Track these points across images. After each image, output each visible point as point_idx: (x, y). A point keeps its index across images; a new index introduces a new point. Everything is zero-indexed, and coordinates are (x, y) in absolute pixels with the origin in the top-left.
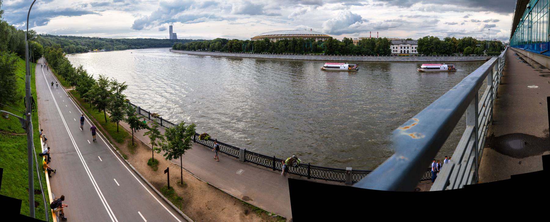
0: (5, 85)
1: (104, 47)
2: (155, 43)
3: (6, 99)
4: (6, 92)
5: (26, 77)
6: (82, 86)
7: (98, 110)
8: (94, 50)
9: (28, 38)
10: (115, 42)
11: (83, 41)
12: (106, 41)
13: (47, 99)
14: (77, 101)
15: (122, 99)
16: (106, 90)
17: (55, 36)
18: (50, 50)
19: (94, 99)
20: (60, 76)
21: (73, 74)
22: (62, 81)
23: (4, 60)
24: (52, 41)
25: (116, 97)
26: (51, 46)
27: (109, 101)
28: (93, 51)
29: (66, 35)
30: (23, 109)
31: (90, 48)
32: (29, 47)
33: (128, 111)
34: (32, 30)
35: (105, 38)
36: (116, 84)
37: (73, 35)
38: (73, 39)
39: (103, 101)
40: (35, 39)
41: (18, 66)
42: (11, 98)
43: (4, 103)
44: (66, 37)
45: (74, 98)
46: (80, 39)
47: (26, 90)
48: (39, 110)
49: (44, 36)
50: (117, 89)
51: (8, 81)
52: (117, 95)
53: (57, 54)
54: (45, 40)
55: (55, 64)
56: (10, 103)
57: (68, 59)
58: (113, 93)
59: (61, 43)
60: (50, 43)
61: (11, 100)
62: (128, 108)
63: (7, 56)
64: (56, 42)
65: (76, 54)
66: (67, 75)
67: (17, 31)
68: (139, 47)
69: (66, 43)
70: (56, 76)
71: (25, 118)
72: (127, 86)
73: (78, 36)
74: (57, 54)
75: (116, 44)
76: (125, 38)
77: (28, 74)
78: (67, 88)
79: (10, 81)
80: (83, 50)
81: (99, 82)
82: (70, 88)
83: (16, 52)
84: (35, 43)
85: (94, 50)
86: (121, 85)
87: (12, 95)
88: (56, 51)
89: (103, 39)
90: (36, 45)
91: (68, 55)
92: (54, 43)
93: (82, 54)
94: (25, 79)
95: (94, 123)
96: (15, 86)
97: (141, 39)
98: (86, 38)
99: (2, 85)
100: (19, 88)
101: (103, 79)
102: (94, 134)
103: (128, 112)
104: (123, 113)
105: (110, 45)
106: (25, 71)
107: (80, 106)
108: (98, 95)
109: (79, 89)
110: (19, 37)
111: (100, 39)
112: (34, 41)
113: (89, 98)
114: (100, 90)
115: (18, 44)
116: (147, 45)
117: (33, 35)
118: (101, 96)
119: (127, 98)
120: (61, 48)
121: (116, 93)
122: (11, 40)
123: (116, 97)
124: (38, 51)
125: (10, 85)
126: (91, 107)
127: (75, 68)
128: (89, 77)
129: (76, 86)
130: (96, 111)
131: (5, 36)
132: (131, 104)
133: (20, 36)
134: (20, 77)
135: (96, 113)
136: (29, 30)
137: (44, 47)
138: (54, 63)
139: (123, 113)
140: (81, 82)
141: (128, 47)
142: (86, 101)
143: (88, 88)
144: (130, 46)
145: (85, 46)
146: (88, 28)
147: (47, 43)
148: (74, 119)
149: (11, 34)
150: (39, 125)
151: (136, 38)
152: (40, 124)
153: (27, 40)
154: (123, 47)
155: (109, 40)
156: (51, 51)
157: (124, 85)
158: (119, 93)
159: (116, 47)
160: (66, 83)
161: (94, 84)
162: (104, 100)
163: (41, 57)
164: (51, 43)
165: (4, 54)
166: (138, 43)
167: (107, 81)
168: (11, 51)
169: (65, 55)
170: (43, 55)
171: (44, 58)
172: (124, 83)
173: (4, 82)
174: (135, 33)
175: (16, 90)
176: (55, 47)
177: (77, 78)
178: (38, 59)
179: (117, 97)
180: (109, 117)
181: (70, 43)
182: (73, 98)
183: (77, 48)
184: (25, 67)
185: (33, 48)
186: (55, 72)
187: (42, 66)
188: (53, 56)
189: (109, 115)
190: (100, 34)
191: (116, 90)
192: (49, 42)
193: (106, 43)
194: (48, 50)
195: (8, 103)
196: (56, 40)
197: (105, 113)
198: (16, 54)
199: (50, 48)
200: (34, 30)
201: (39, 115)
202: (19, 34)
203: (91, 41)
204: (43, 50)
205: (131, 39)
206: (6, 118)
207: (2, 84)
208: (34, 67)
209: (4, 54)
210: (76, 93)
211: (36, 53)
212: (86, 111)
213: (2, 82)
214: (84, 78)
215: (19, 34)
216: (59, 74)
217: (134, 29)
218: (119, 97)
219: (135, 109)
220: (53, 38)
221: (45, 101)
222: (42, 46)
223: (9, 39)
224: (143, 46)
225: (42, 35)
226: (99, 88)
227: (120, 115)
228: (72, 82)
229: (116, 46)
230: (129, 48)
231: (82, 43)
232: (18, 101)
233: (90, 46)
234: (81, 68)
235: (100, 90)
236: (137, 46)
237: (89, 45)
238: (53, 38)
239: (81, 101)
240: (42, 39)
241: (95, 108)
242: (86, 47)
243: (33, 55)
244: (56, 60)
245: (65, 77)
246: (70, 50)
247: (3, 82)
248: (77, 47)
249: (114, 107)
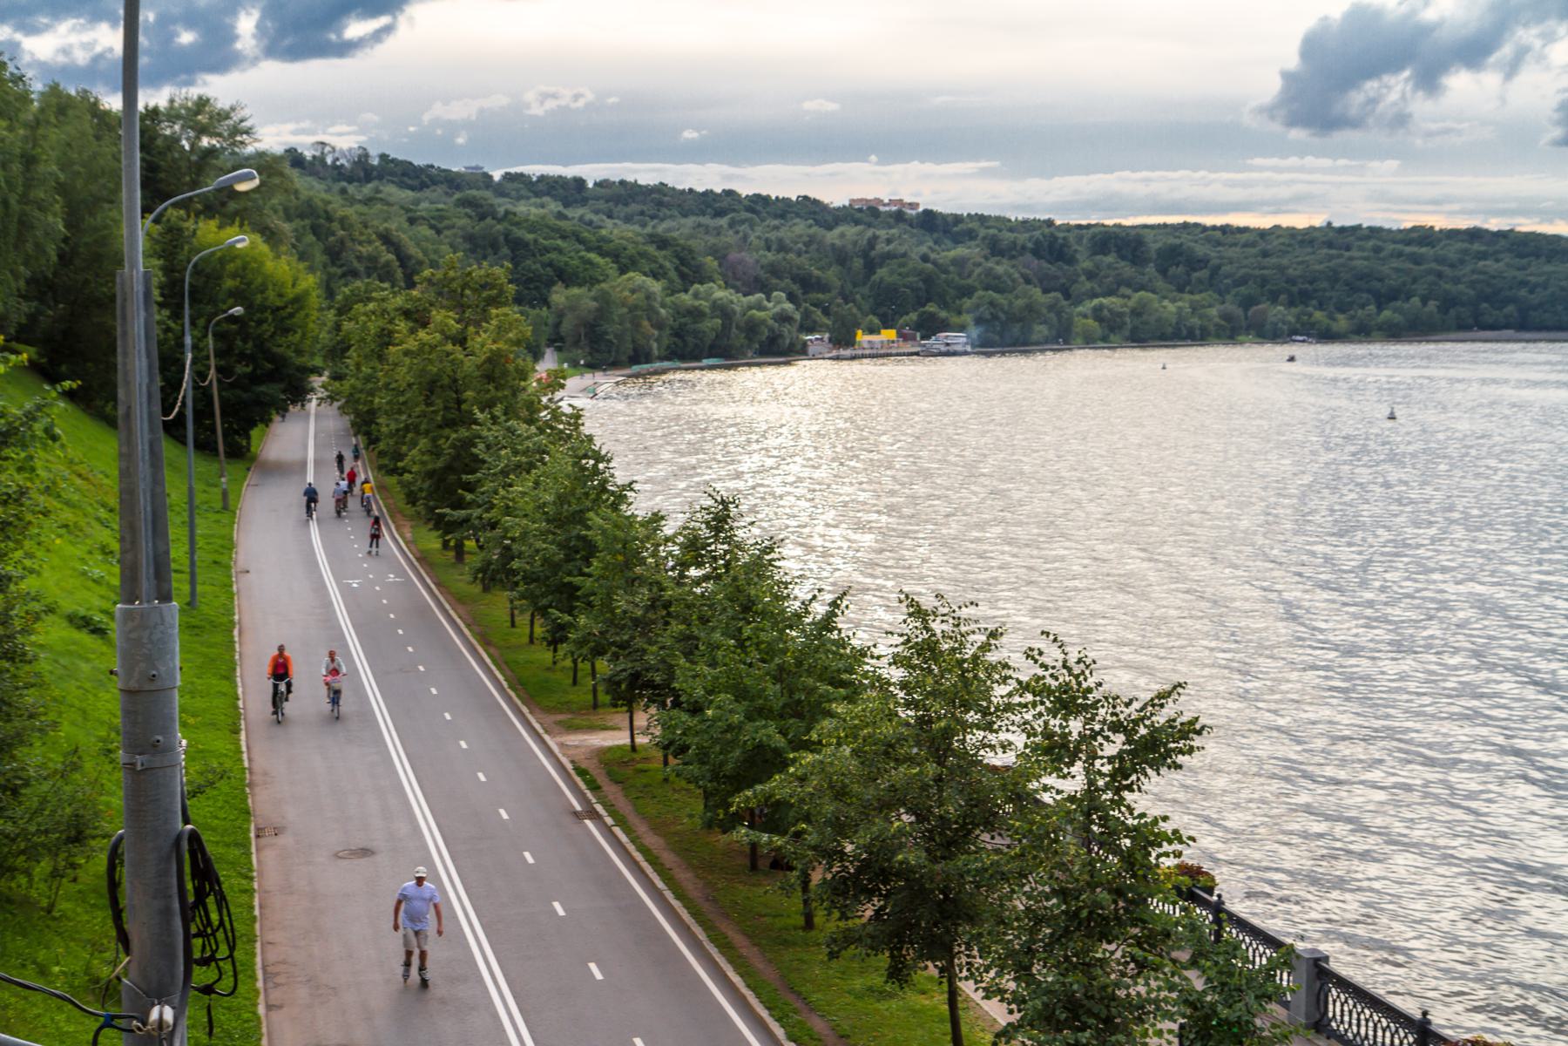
1: (967, 303)
2: (1523, 283)
6: (723, 708)
7: (884, 959)
8: (862, 337)
9: (155, 191)
10: (1086, 264)
12: (996, 249)
13: (359, 841)
14: (668, 858)
15: (1135, 862)
16: (970, 762)
17: (452, 181)
18: (402, 326)
19: (849, 848)
20: (499, 604)
21: (632, 583)
24: (424, 231)
25: (1069, 841)
26: (411, 285)
27: (1004, 877)
29: (569, 172)
31: (818, 314)
33: (1199, 985)
34: (202, 103)
35: (982, 219)
36: (1085, 708)
37: (645, 174)
39: (937, 867)
40: (232, 206)
45: (642, 829)
46: (719, 213)
47: (130, 767)
48: (272, 956)
49: (338, 173)
50: (1093, 756)
53: (469, 365)
54: (350, 211)
55: (452, 478)
57: (586, 430)
58: (1046, 798)
59: (517, 245)
62: (1194, 963)
64: (470, 238)
66: (569, 596)
67: (25, 98)
68: (1342, 322)
69: (571, 255)
70: (458, 600)
72: (1191, 729)
73: (700, 189)
74: (469, 365)
75: (1091, 275)
76: (1192, 219)
77: (146, 584)
80: (752, 328)
81: (897, 674)
84: (242, 240)
85: (862, 337)
86: (1125, 713)
88: (461, 341)
89: (958, 219)
90: (246, 267)
91: (588, 379)
92: (445, 248)
97: (1375, 232)
98: (783, 209)
101: (946, 646)
103: (1192, 1002)
105: (1037, 292)
107: (695, 914)
108: (886, 806)
109: (692, 740)
110: (49, 167)
111: (930, 221)
112: (228, 219)
113: (798, 835)
115: (39, 247)
116: (1432, 305)
117: (211, 152)
118: (921, 818)
119: (1190, 856)
120: (512, 312)
121: (1072, 799)
123: (1069, 841)
126: (809, 924)
127: (657, 518)
132: (1231, 915)
134: (68, 606)
135: (858, 983)
136: (141, 107)
137: (330, 293)
138: (440, 464)
141: (1227, 317)
142: (764, 864)
143: (783, 733)
144: (1248, 302)
145: (767, 290)
146: (808, 105)
147: (365, 250)
151: (1318, 221)
153: (146, 210)
154: (1169, 308)
155: (1022, 238)
156: (409, 339)
157: (1160, 719)
159: (1097, 314)
160: (558, 676)
161: (851, 699)
163: (299, 394)
164: (413, 250)
166: (1334, 277)
171: (331, 410)
172: (1163, 695)
174: (1301, 170)
175: (20, 752)
177: (677, 627)
178: (267, 422)
182: (628, 831)
183: (679, 312)
185: (213, 301)
187: (311, 496)
188: (431, 387)
189: (999, 1013)
190: (929, 167)
191: (1078, 767)
192: (386, 239)
193: (989, 272)
194: (373, 327)
196: (462, 221)
197: (953, 994)
199: (399, 301)
200: (223, 103)
201: (269, 1007)
202: (54, 135)
203: (832, 237)
204: (319, 323)
205: (1263, 234)
208: (227, 506)
210: (666, 780)
211: (242, 357)
214: (747, 632)
216: (492, 577)
217: (1293, 121)
218: (1108, 841)
219: (1269, 972)
221: (337, 856)
222: (309, 281)
224: (1387, 314)
225: (308, 154)
226: (901, 739)
227: (1108, 1021)
230: (1229, 332)
232: (43, 867)
234: (721, 520)
235: (911, 760)
236: (1321, 307)
237: (807, 283)
238: (429, 202)
240: (309, 203)
241: (848, 939)
242: (779, 303)
244: (464, 433)
246: (611, 329)
248: (686, 298)
249: (1054, 940)
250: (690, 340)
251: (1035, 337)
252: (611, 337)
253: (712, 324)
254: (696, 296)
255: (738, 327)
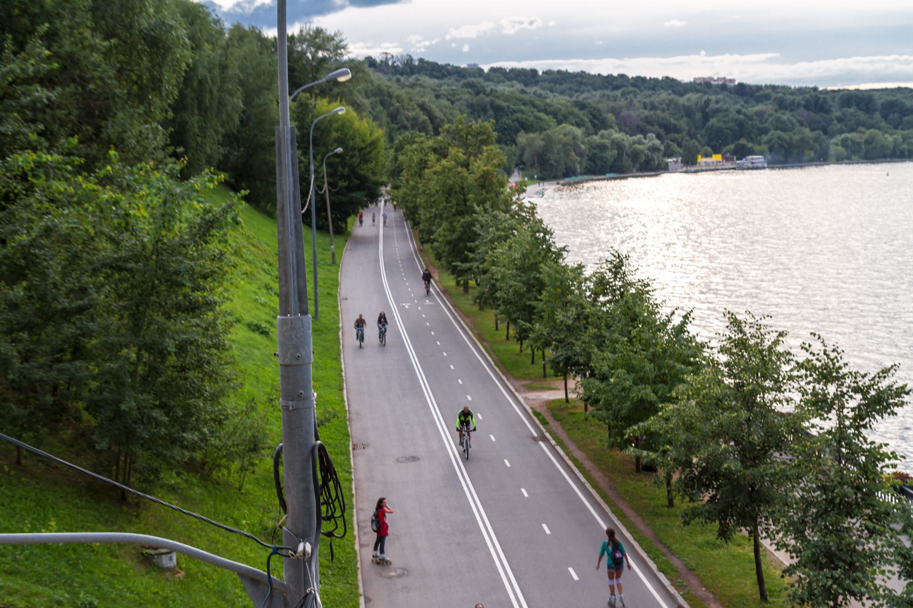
0: (154, 371)
1: (765, 138)
3: (158, 455)
4: (158, 414)
5: (284, 323)
7: (716, 525)
8: (701, 159)
11: (631, 103)
12: (782, 105)
14: (588, 464)
15: (868, 470)
16: (766, 410)
17: (459, 73)
18: (432, 157)
20: (489, 317)
21: (566, 304)
22: (502, 348)
23: (141, 214)
25: (828, 458)
26: (437, 133)
27: (788, 478)
28: (694, 162)
29: (526, 65)
30: (266, 511)
31: (675, 146)
32: (302, 142)
34: (319, 32)
35: (774, 88)
36: (837, 378)
37: (571, 66)
38: (571, 92)
39: (748, 472)
40: (336, 90)
41: (236, 253)
42: (193, 447)
43: (150, 480)
44: (528, 77)
45: (572, 447)
46: (616, 88)
47: (286, 408)
50: (842, 407)
51: (172, 349)
52: (839, 442)
53: (471, 179)
55: (461, 245)
56: (187, 481)
57: (538, 217)
58: (814, 432)
59: (498, 111)
60: (429, 113)
61: (192, 459)
62: (904, 531)
63: (162, 195)
65: (586, 185)
66: (529, 313)
67: (221, 32)
69: (529, 114)
70: (465, 315)
71: (281, 573)
72: (902, 391)
74: (471, 179)
75: (840, 120)
77: (293, 304)
78: (531, 389)
79: (182, 349)
80: (635, 155)
81: (724, 358)
82: (550, 389)
83: (220, 167)
84: (341, 110)
85: (701, 159)
86: (863, 382)
87: (199, 430)
88: (466, 165)
89: (759, 88)
90: (344, 125)
92: (456, 112)
93: (624, 182)
94: (275, 333)
95: (685, 599)
96: (212, 376)
98: (653, 85)
99: (133, 375)
100: (242, 385)
102: (616, 566)
104: (871, 558)
105: (807, 131)
106: (276, 286)
107: (604, 497)
110: (234, 71)
111: (743, 90)
112: (333, 98)
113: (665, 452)
114: (731, 409)
115: (229, 116)
117: (324, 59)
120: (495, 148)
121: (829, 432)
122: (188, 92)
123: (828, 458)
124: (356, 160)
125: (183, 369)
126: (671, 504)
127: (581, 267)
128: (665, 324)
129: (585, 375)
130: (702, 533)
131: (145, 62)
133: (242, 69)
134: (247, 318)
135: (700, 539)
137: (391, 139)
138: (455, 236)
139: (871, 558)
140: (614, 352)
145: (644, 133)
147: (411, 114)
148: (571, 570)
149: (184, 55)
150: (362, 600)
152: (370, 595)
154: (889, 139)
155: (798, 98)
156: (436, 165)
157: (884, 384)
158: (852, 431)
159: (844, 143)
160: (523, 358)
161: (696, 373)
162: (755, 466)
163: (373, 197)
164: (438, 114)
165: (148, 183)
167: (779, 355)
168: (185, 161)
169: (520, 189)
170: (383, 189)
173: (146, 355)
176: (461, 138)
177: (592, 330)
179: (839, 457)
180: (779, 573)
181: (555, 114)
182: (564, 448)
183: (592, 146)
184: (274, 259)
186: (461, 289)
188: (449, 192)
189: (785, 559)
190: (736, 57)
191: (833, 415)
192: (423, 107)
193: (778, 119)
194: (416, 159)
195: (170, 477)
196: (466, 96)
197: (757, 547)
198: (222, 176)
199: (431, 143)
200: (330, 32)
201: (361, 546)
202: (237, 53)
204: (385, 156)
206: (162, 570)
207: (135, 364)
208: (334, 262)
209: (148, 183)
210: (586, 419)
212: (641, 526)
213: (133, 356)
214: (634, 333)
215: (237, 53)
216: (484, 302)
220: (447, 85)
222: (379, 133)
223: (171, 84)
227: (851, 564)
228: (561, 352)
229: (841, 132)
231: (625, 113)
232: (236, 465)
233: (672, 135)
234: (618, 266)
235: (731, 409)
237: (668, 128)
238: (447, 85)
239: (609, 470)
240: (379, 88)
242: (652, 140)
243: (326, 186)
244: (468, 218)
245: (521, 322)
246: (553, 157)
247: (139, 356)
248: (596, 138)
249: (818, 516)
250: (599, 163)
251: (806, 158)
252: (552, 162)
253: (611, 153)
254: (602, 137)
255: (627, 155)
